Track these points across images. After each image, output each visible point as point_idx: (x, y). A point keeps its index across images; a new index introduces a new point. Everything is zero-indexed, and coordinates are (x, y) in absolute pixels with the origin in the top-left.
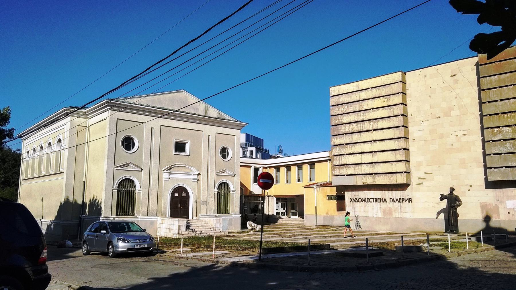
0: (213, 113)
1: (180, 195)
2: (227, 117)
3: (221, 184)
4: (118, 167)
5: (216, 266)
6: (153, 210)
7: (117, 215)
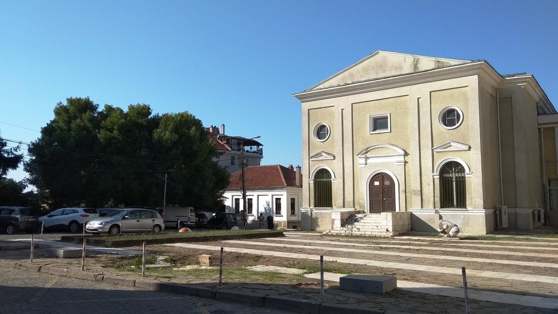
0: (427, 63)
1: (382, 183)
2: (453, 62)
3: (317, 173)
4: (313, 157)
5: (305, 271)
6: (349, 202)
7: (315, 206)
